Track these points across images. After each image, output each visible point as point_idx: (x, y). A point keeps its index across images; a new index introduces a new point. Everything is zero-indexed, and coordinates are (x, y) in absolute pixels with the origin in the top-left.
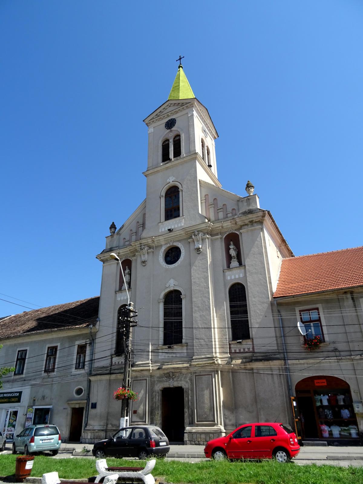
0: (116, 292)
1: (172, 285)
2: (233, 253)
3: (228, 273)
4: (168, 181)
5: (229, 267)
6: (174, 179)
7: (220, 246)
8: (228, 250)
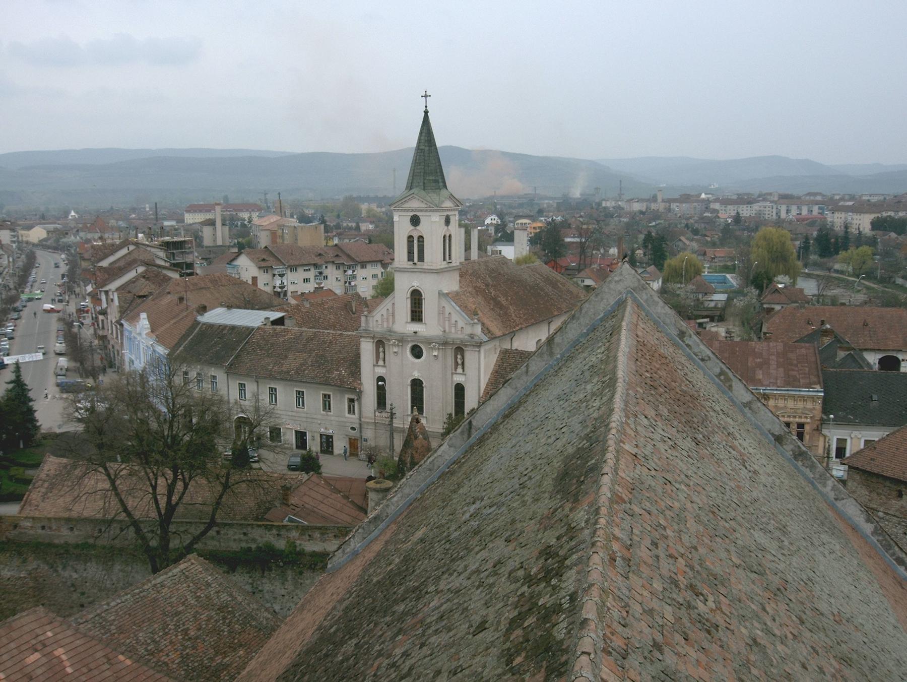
1: (416, 375)
2: (460, 362)
3: (454, 376)
5: (456, 370)
7: (450, 353)
8: (456, 358)
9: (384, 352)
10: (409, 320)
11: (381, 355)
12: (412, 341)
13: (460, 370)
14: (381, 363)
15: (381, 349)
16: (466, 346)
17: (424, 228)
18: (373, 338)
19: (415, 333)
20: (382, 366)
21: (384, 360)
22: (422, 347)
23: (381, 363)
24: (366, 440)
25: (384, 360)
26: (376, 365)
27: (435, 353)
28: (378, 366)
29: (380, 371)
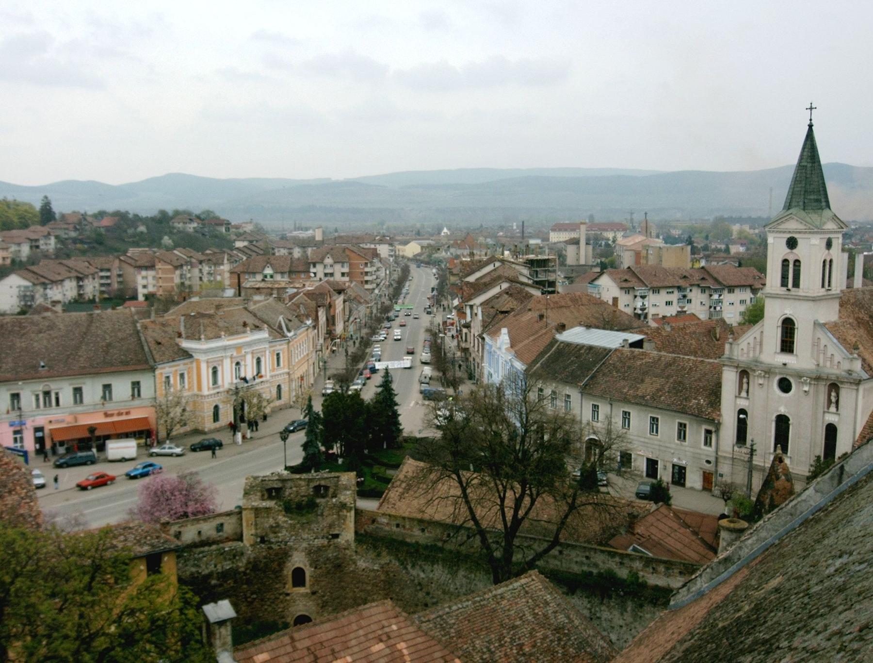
0: (736, 397)
1: (783, 410)
2: (833, 399)
4: (786, 312)
6: (791, 312)
8: (829, 395)
9: (748, 383)
10: (779, 349)
11: (745, 386)
12: (780, 374)
13: (833, 409)
14: (744, 394)
15: (745, 380)
16: (842, 383)
17: (800, 252)
18: (737, 367)
19: (785, 364)
20: (745, 398)
21: (748, 392)
22: (791, 380)
23: (744, 394)
24: (721, 475)
25: (748, 392)
26: (738, 396)
27: (806, 388)
28: (741, 397)
29: (743, 403)
